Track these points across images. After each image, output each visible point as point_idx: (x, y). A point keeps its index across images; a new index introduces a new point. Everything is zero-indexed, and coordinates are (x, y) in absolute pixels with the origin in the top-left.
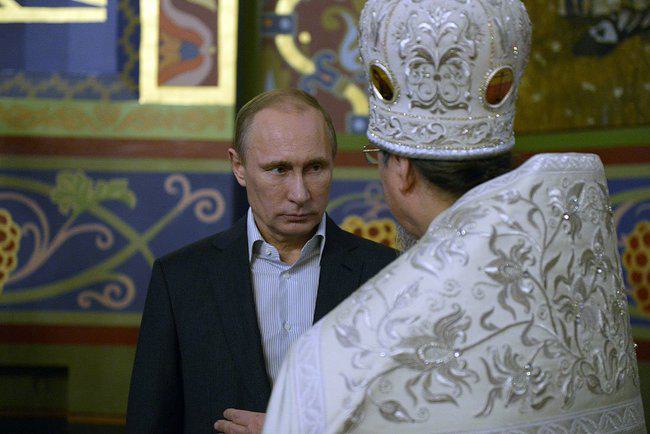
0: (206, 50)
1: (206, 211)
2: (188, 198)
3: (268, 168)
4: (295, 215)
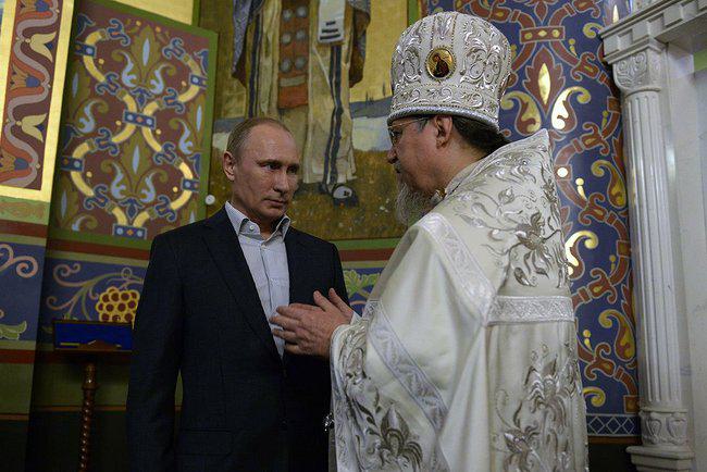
0: (34, 165)
1: (23, 270)
2: (11, 261)
3: (262, 164)
4: (277, 201)
